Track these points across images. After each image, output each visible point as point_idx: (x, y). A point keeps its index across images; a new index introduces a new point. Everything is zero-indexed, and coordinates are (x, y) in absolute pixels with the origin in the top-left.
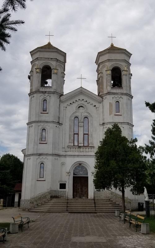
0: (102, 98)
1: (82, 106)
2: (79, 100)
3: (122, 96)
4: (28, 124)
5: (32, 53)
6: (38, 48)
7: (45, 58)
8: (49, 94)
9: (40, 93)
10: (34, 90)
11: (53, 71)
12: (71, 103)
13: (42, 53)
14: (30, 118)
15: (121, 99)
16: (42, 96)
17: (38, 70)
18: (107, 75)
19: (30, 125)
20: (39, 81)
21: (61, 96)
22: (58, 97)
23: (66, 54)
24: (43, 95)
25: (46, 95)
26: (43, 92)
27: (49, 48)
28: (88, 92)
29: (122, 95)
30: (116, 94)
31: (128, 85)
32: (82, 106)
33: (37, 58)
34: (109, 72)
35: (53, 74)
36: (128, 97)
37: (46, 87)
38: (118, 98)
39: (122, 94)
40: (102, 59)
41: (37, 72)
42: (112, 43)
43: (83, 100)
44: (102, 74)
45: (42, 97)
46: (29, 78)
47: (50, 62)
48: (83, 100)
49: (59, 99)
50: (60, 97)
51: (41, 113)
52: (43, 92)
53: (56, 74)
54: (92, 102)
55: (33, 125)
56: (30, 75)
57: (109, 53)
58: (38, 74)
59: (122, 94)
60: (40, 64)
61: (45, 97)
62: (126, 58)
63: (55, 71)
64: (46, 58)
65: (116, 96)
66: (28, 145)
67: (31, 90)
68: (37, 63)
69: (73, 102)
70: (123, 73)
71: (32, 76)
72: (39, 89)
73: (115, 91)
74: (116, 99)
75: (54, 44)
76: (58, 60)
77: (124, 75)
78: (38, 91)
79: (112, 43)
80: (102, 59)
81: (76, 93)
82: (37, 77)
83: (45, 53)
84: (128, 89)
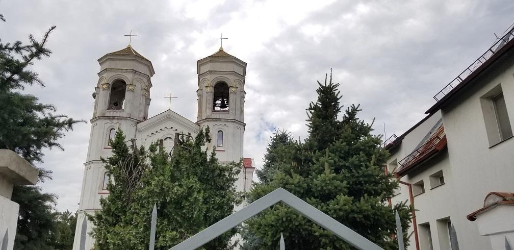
0: (199, 126)
1: (170, 138)
2: (161, 130)
3: (227, 124)
4: (85, 164)
5: (101, 61)
6: (107, 55)
7: (116, 69)
8: (119, 121)
9: (105, 119)
10: (98, 115)
11: (127, 87)
12: (152, 134)
13: (113, 62)
14: (89, 155)
15: (225, 128)
16: (108, 124)
17: (105, 87)
18: (207, 93)
19: (88, 166)
20: (105, 102)
21: (138, 123)
22: (134, 125)
23: (151, 62)
24: (110, 122)
25: (115, 121)
26: (109, 118)
27: (129, 55)
28: (179, 117)
29: (227, 122)
30: (211, 121)
31: (238, 107)
32: (170, 138)
33: (106, 69)
34: (211, 89)
35: (128, 91)
36: (236, 125)
37: (215, 105)
38: (220, 127)
39: (227, 120)
40: (205, 69)
41: (104, 89)
42: (221, 47)
43: (172, 128)
44: (201, 91)
45: (108, 125)
46: (94, 96)
47: (124, 74)
48: (172, 128)
49: (135, 127)
50: (136, 125)
51: (105, 148)
52: (109, 118)
53: (133, 91)
54: (158, 129)
55: (92, 165)
56: (95, 92)
57: (211, 61)
58: (105, 92)
59: (227, 120)
60: (109, 78)
61: (113, 124)
62: (239, 70)
63: (131, 88)
64: (118, 69)
65: (218, 123)
66: (83, 196)
67: (95, 114)
68: (105, 75)
69: (157, 132)
70: (231, 90)
71: (98, 94)
72: (104, 114)
73: (111, 114)
74: (219, 127)
75: (134, 47)
76: (136, 71)
77: (231, 93)
78: (103, 117)
79: (221, 47)
80: (205, 69)
81: (160, 119)
82: (105, 97)
83: (118, 62)
84: (238, 112)
